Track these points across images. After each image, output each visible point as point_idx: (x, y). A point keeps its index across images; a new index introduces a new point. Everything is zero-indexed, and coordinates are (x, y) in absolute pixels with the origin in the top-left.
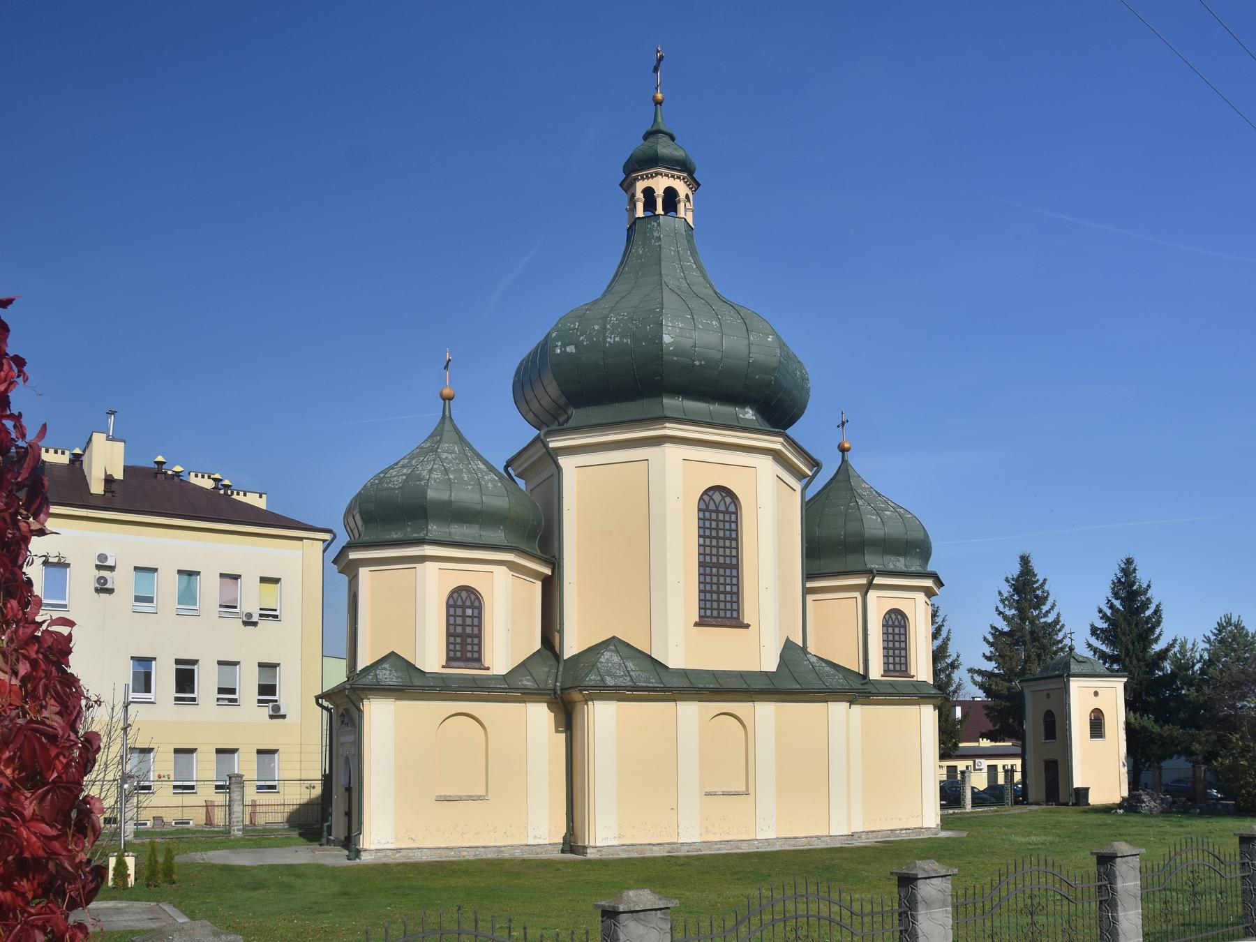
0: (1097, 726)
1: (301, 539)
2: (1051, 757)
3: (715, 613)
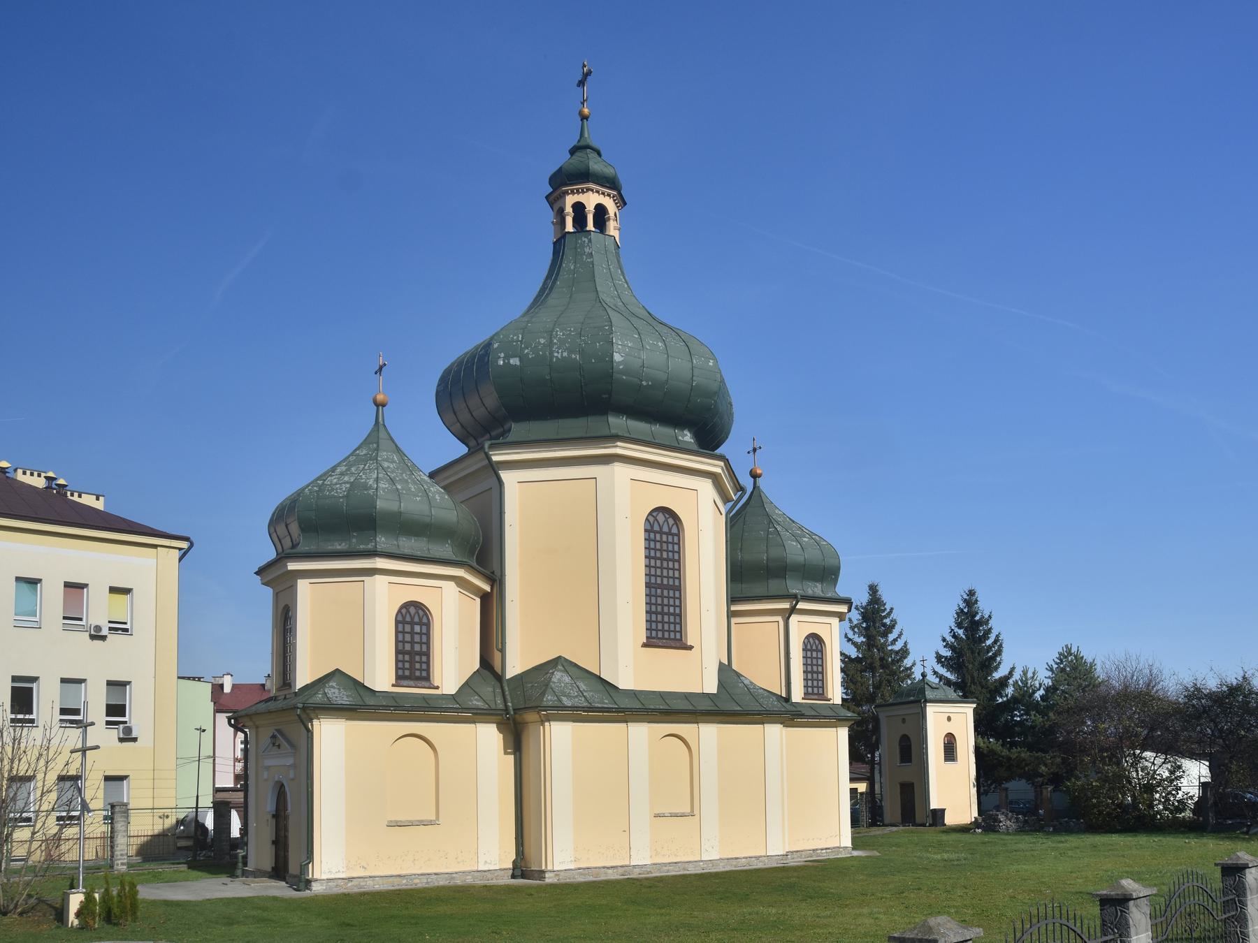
0: (950, 751)
1: (155, 546)
2: (907, 779)
3: (660, 635)
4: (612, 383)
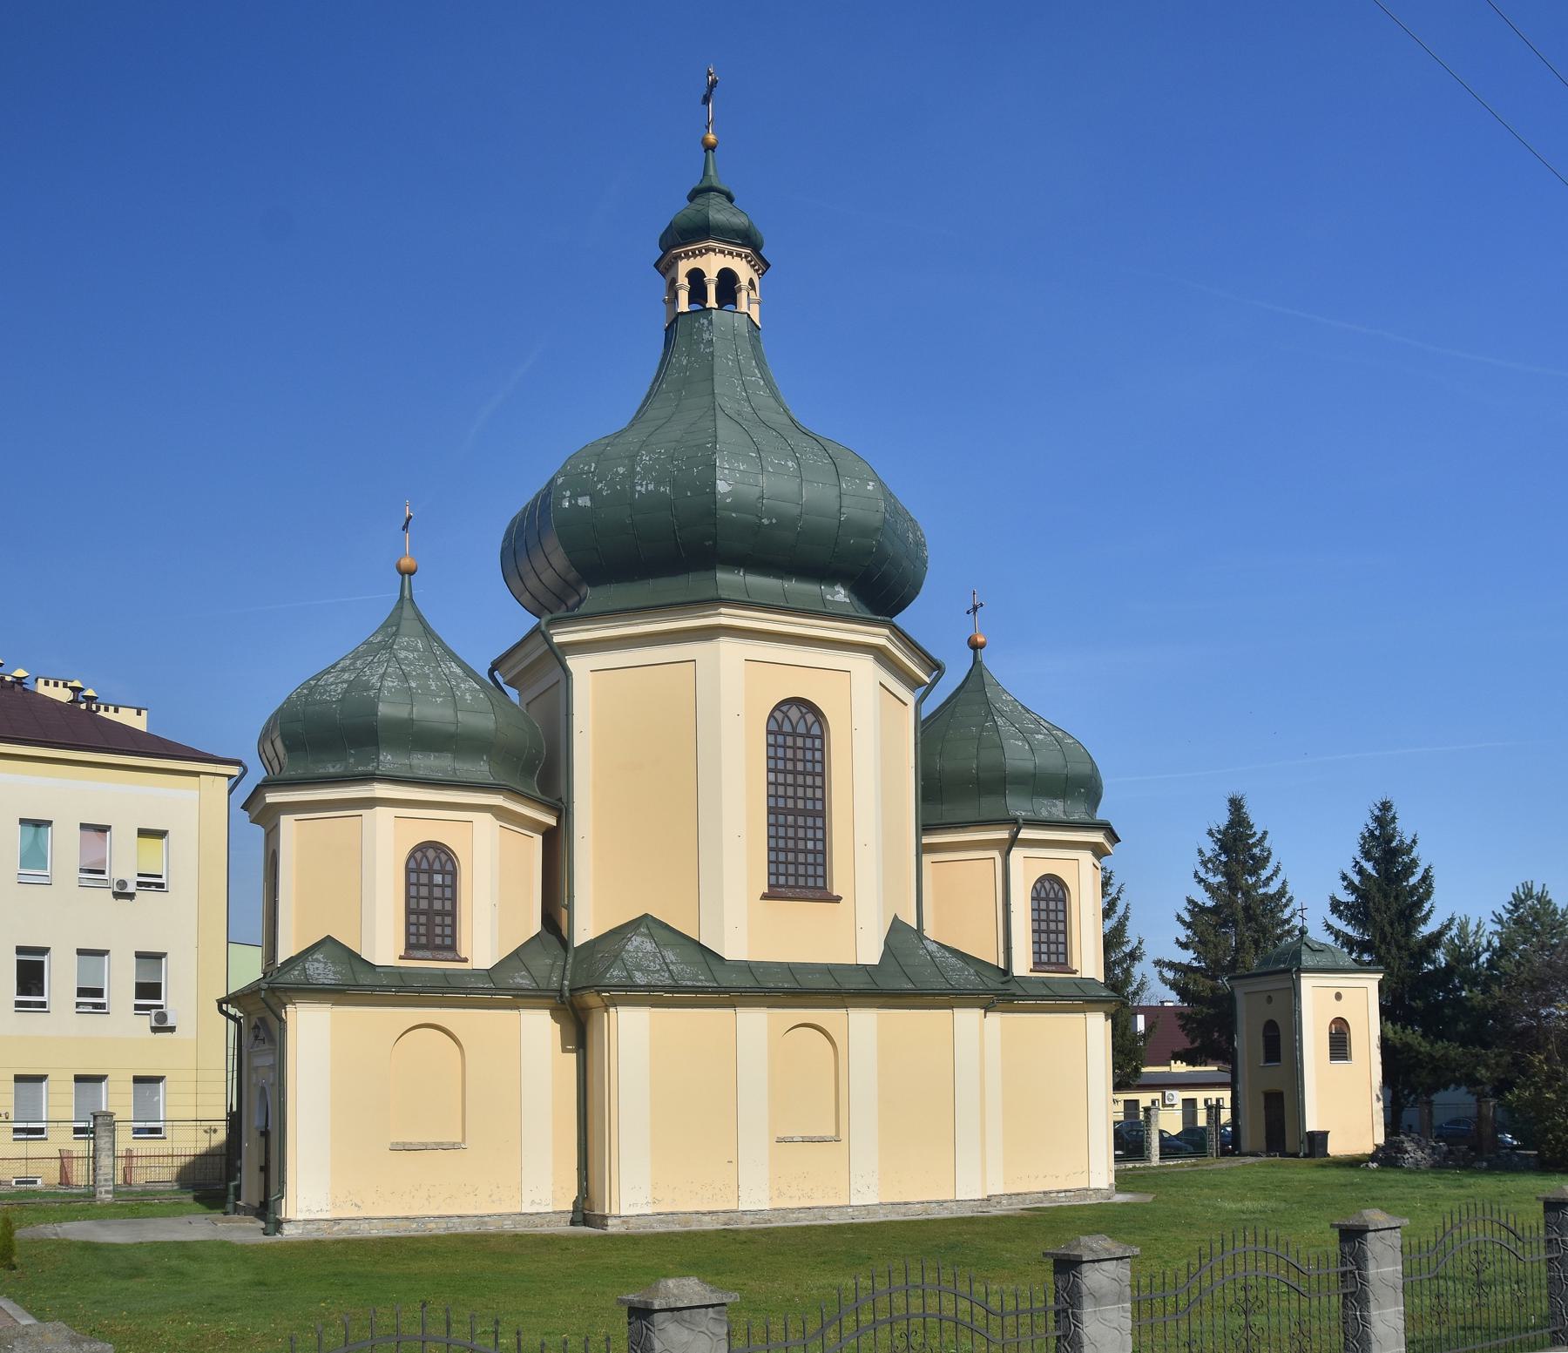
0: (1339, 1044)
1: (197, 774)
3: (791, 881)
4: (715, 524)
